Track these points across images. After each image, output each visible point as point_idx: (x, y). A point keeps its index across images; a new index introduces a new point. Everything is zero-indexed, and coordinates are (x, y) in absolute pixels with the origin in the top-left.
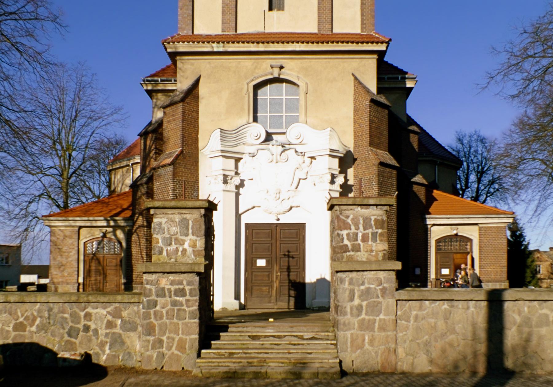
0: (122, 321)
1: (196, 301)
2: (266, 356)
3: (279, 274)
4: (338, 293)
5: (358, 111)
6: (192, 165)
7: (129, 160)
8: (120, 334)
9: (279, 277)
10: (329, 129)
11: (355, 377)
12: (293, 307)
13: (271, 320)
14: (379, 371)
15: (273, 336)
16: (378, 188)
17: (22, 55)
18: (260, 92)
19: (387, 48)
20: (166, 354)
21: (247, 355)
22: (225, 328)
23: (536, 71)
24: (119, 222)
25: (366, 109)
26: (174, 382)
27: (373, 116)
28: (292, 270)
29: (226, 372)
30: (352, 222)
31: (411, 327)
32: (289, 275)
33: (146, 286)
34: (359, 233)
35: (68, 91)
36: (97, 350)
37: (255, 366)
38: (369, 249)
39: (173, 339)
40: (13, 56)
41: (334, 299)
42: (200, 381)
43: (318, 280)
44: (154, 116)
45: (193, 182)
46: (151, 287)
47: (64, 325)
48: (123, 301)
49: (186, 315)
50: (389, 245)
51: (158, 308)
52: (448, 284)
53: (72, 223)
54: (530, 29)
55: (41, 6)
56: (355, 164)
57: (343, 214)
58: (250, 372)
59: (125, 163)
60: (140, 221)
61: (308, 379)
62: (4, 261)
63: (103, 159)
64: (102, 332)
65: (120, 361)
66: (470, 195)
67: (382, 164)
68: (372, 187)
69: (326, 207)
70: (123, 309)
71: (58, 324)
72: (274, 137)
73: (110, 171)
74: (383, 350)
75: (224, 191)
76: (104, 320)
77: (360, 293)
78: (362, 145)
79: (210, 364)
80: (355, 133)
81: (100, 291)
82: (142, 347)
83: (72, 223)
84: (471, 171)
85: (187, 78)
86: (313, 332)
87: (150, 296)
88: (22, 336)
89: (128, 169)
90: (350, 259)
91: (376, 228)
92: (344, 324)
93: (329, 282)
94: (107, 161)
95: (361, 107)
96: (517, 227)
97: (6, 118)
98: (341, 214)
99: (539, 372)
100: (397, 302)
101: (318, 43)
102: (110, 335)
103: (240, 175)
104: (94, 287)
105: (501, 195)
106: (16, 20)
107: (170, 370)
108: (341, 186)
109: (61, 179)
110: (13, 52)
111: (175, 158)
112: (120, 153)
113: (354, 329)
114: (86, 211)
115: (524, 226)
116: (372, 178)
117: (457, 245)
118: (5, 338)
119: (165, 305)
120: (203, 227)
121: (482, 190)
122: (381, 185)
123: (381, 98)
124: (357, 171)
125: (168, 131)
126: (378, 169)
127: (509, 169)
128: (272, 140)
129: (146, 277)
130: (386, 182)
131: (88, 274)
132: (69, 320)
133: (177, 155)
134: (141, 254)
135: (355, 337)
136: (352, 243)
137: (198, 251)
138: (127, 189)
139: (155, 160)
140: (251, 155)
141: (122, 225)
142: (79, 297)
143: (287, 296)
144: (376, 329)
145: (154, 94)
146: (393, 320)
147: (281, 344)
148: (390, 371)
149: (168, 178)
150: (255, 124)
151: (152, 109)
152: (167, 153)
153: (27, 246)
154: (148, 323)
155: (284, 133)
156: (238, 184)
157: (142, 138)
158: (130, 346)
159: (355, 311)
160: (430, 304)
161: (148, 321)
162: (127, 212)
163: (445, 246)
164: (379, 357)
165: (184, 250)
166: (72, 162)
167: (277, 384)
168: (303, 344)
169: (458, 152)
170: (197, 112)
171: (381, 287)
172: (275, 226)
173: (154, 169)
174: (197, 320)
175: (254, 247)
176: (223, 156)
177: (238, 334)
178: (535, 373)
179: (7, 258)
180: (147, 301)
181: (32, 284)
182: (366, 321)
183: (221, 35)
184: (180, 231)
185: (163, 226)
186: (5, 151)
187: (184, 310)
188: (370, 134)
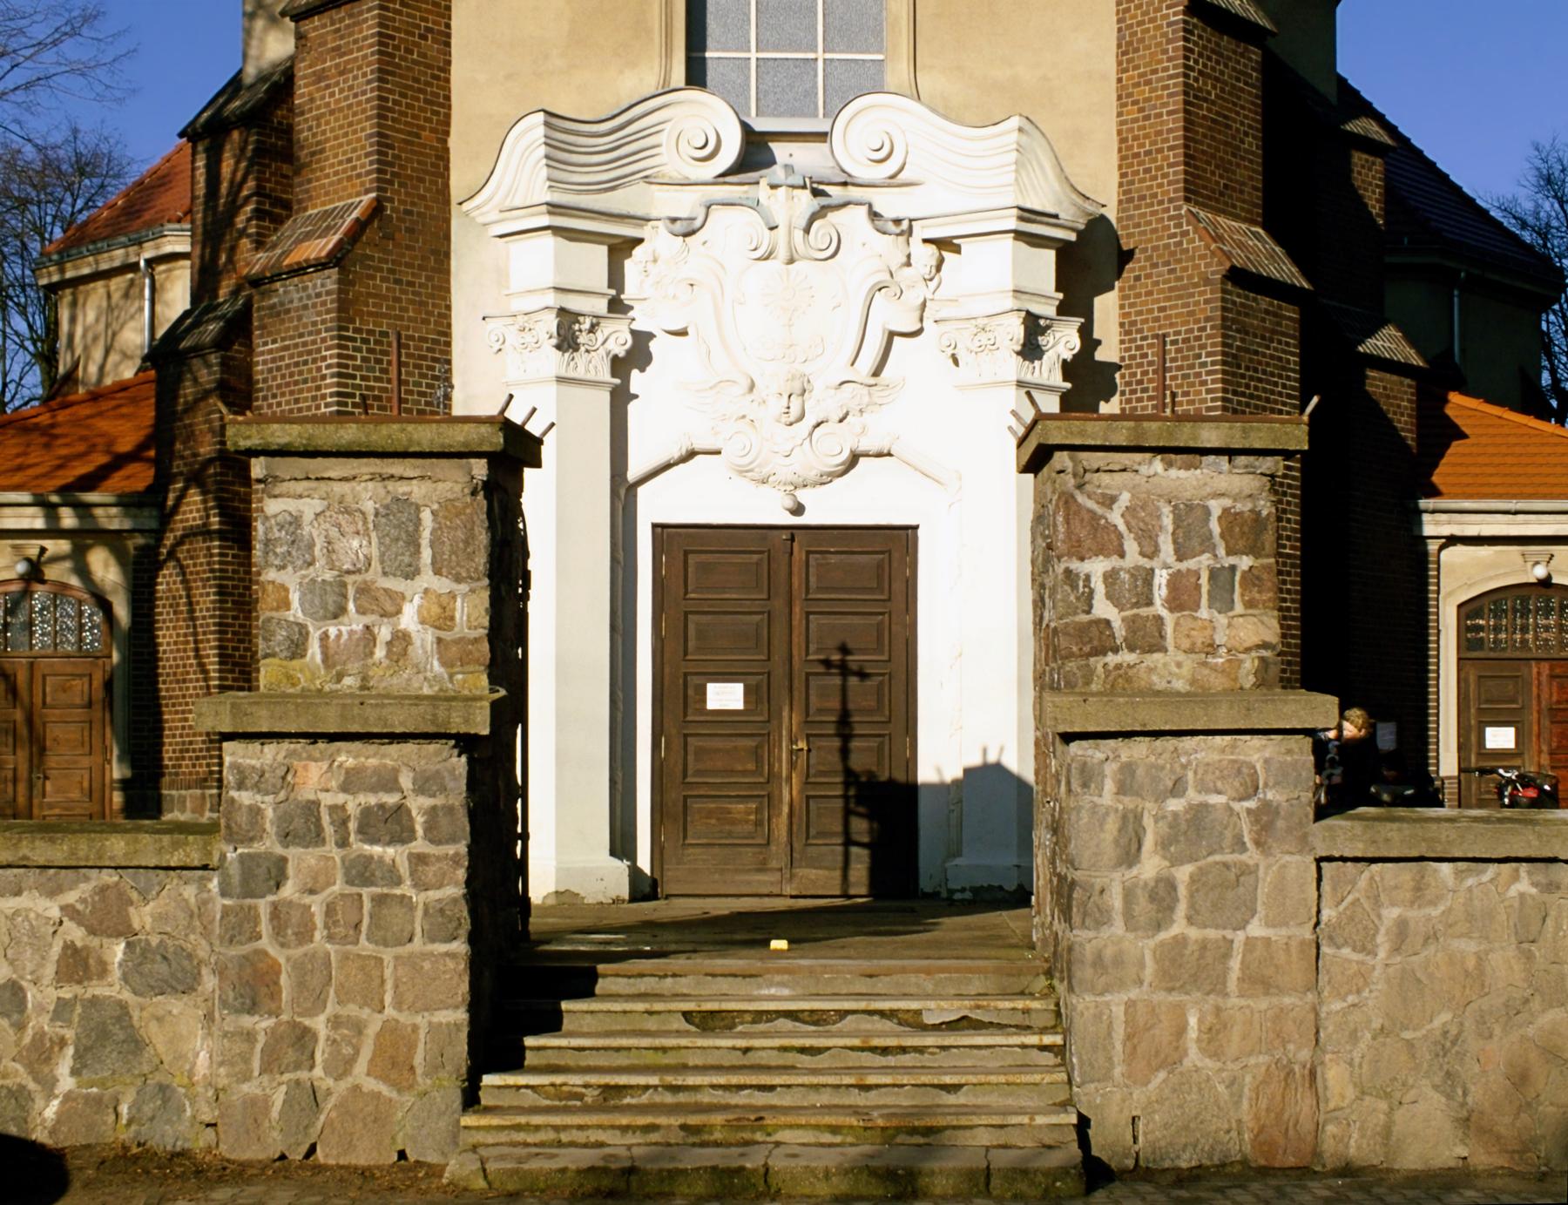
0: (129, 945)
1: (455, 860)
3: (802, 745)
5: (1136, 50)
6: (421, 268)
7: (139, 243)
8: (123, 1006)
9: (802, 760)
12: (864, 891)
13: (779, 944)
14: (1244, 1162)
16: (1223, 381)
20: (329, 1093)
21: (682, 1098)
22: (581, 982)
24: (99, 512)
25: (1169, 42)
27: (1200, 72)
29: (592, 1169)
30: (1128, 524)
32: (845, 752)
33: (234, 794)
34: (1157, 572)
37: (717, 1144)
38: (1200, 638)
39: (358, 1028)
41: (1054, 852)
43: (967, 771)
44: (253, 52)
45: (425, 340)
46: (259, 798)
48: (135, 863)
49: (412, 922)
50: (1282, 626)
51: (289, 891)
52: (1532, 793)
56: (1125, 275)
57: (1088, 487)
59: (118, 256)
60: (194, 509)
67: (1238, 277)
68: (1198, 375)
69: (1008, 455)
70: (134, 895)
72: (779, 150)
73: (53, 288)
75: (561, 380)
76: (51, 945)
78: (1155, 196)
79: (520, 1137)
80: (1122, 141)
82: (221, 1064)
86: (959, 996)
87: (252, 840)
89: (132, 282)
91: (1229, 553)
94: (35, 246)
95: (1148, 30)
98: (1080, 487)
100: (1319, 869)
102: (79, 1009)
103: (631, 314)
108: (1069, 369)
111: (346, 234)
112: (92, 211)
113: (1141, 982)
116: (1198, 338)
117: (1547, 628)
119: (322, 879)
120: (483, 538)
122: (1234, 364)
124: (1132, 305)
125: (318, 118)
126: (1223, 300)
130: (1256, 353)
133: (357, 220)
134: (197, 656)
137: (461, 640)
138: (128, 373)
139: (259, 244)
140: (678, 227)
141: (115, 525)
143: (840, 840)
144: (1232, 984)
146: (1303, 943)
147: (828, 1049)
148: (1291, 1161)
149: (314, 324)
150: (695, 94)
151: (240, 21)
154: (245, 957)
155: (822, 137)
156: (621, 352)
157: (200, 148)
159: (1142, 905)
160: (1457, 873)
161: (247, 948)
162: (133, 468)
163: (1497, 629)
164: (1245, 1104)
165: (401, 639)
168: (920, 1050)
169: (1544, 232)
170: (445, 40)
171: (1251, 804)
172: (785, 535)
173: (256, 282)
174: (460, 947)
175: (691, 627)
176: (557, 231)
177: (640, 1006)
184: (382, 555)
185: (307, 529)
188: (1186, 147)
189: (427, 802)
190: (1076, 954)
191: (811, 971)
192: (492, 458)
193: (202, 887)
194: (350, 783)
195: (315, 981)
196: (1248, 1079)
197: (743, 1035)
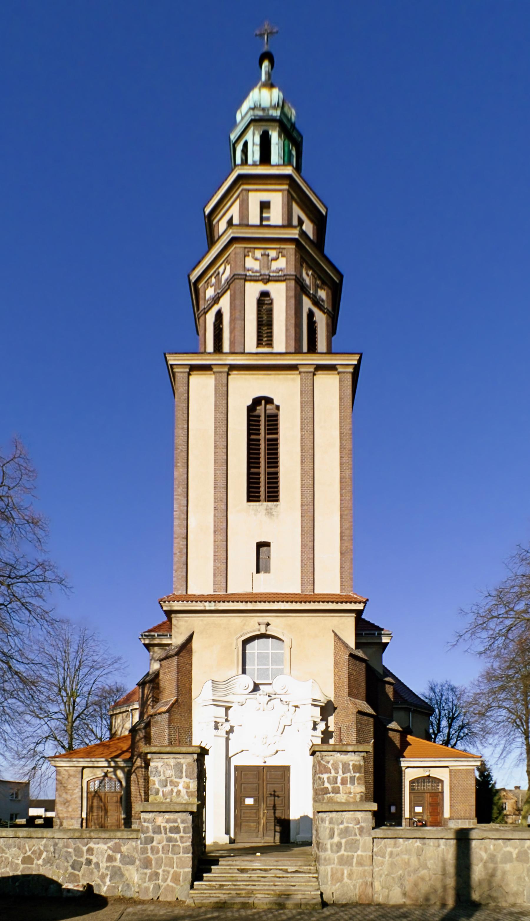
0: (121, 855)
1: (189, 837)
2: (253, 887)
3: (266, 811)
4: (319, 832)
7: (129, 706)
9: (266, 814)
10: (312, 680)
11: (335, 908)
13: (258, 854)
14: (357, 903)
15: (260, 870)
17: (31, 614)
18: (248, 646)
19: (364, 607)
20: (162, 886)
21: (236, 887)
22: (215, 862)
23: (500, 630)
24: (119, 763)
26: (169, 912)
28: (277, 808)
29: (217, 903)
31: (386, 863)
32: (274, 813)
33: (143, 823)
35: (72, 643)
36: (99, 881)
37: (243, 897)
38: (348, 791)
39: (169, 872)
40: (23, 615)
42: (193, 910)
43: (301, 817)
47: (69, 859)
51: (154, 844)
52: (420, 824)
53: (76, 764)
54: (494, 593)
55: (48, 570)
58: (239, 903)
59: (124, 709)
60: (139, 762)
61: (291, 909)
62: (14, 796)
63: (105, 704)
64: (103, 865)
65: (119, 892)
66: (442, 739)
67: (360, 713)
69: (308, 753)
70: (122, 844)
71: (63, 858)
72: (261, 687)
73: (111, 716)
74: (361, 883)
75: (215, 736)
77: (339, 831)
79: (202, 895)
80: (335, 684)
81: (103, 827)
83: (76, 764)
84: (443, 717)
85: (181, 634)
86: (296, 866)
87: (147, 833)
88: (29, 868)
89: (127, 714)
90: (331, 801)
91: (354, 773)
92: (325, 859)
93: (312, 820)
94: (108, 707)
96: (485, 768)
97: (16, 669)
98: (322, 759)
99: (504, 904)
101: (301, 602)
102: (111, 868)
104: (96, 821)
105: (470, 739)
106: (26, 582)
107: (165, 900)
108: (323, 733)
109: (66, 722)
110: (23, 611)
113: (334, 863)
114: (89, 753)
115: (491, 767)
118: (14, 871)
120: (196, 770)
121: (453, 735)
122: (359, 731)
123: (359, 652)
127: (478, 715)
128: (259, 690)
129: (143, 815)
131: (90, 809)
132: (73, 854)
135: (334, 871)
136: (332, 786)
137: (191, 792)
139: (153, 707)
140: (240, 704)
142: (81, 834)
144: (354, 864)
145: (151, 648)
146: (369, 856)
148: (367, 902)
150: (244, 675)
151: (149, 661)
152: (163, 701)
153: (35, 783)
155: (270, 684)
156: (228, 730)
158: (129, 878)
159: (335, 848)
160: (404, 842)
161: (145, 856)
162: (126, 754)
163: (418, 786)
164: (357, 890)
166: (76, 708)
167: (263, 913)
168: (287, 877)
169: (431, 700)
170: (191, 665)
171: (358, 826)
173: (151, 716)
174: (190, 855)
176: (214, 705)
177: (228, 867)
178: (500, 905)
179: (17, 794)
180: (145, 837)
181: (40, 817)
182: (345, 856)
183: (212, 595)
185: (159, 769)
186: (15, 698)
187: (178, 846)
189: (183, 825)
190: (320, 857)
191: (264, 860)
192: (198, 754)
193: (136, 842)
194: (168, 821)
195: (160, 862)
196: (358, 885)
197: (250, 874)
